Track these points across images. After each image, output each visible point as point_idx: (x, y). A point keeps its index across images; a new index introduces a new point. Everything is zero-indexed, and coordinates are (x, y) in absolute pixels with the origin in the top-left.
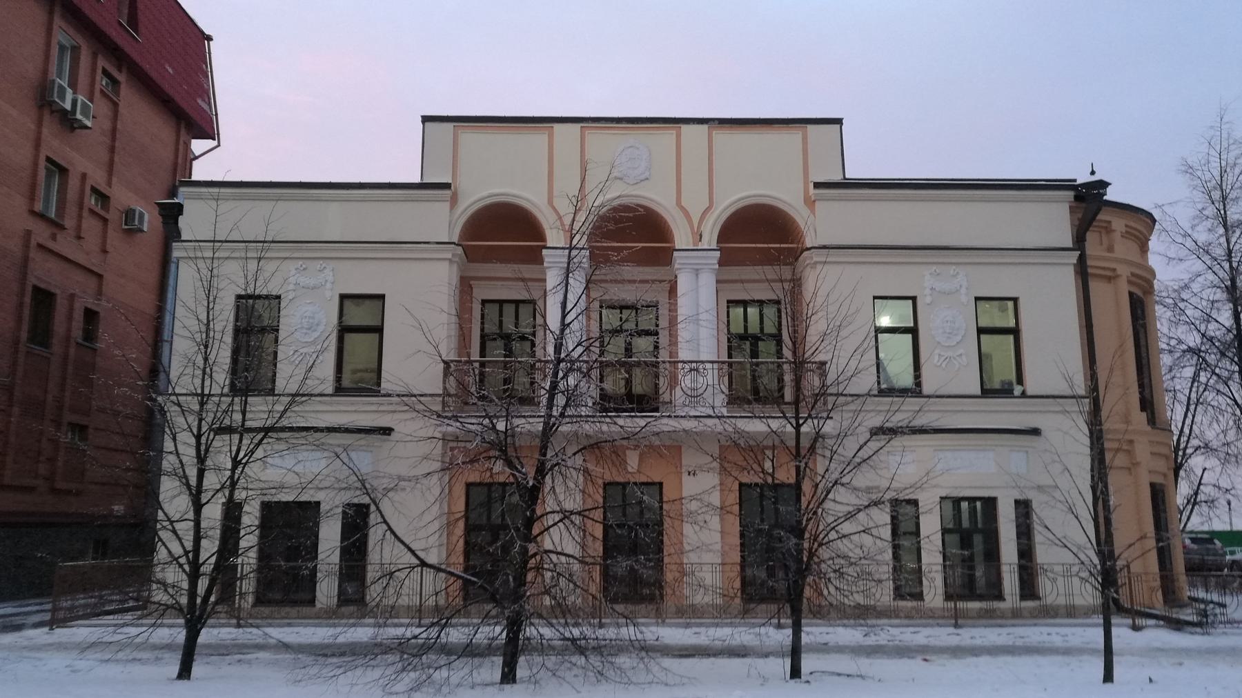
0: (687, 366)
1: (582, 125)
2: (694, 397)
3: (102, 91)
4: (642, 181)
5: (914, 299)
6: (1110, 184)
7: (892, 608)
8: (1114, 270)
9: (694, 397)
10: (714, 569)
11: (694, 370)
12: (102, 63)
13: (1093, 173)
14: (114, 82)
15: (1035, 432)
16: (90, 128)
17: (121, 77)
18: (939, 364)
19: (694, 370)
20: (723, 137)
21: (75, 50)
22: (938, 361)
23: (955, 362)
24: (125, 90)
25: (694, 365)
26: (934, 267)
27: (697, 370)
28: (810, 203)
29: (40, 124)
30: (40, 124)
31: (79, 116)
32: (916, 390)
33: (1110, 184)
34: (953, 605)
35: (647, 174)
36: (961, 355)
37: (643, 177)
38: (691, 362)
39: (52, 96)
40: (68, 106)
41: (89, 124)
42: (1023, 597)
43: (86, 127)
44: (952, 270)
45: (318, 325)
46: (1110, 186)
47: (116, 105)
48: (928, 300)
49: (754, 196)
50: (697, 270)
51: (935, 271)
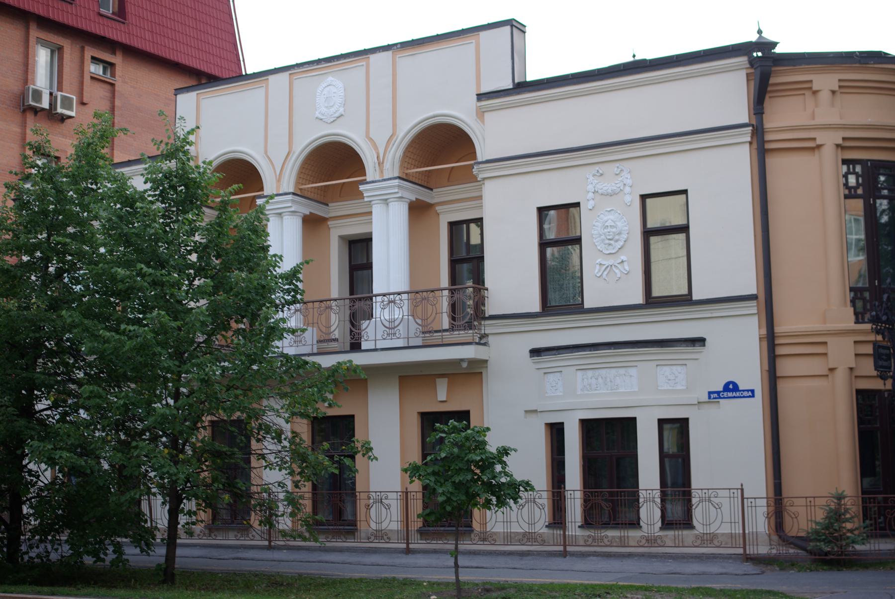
0: (386, 299)
1: (290, 72)
2: (392, 329)
3: (92, 78)
4: (338, 118)
5: (644, 197)
6: (778, 43)
7: (653, 538)
8: (814, 139)
9: (392, 329)
10: (809, 504)
11: (392, 302)
12: (90, 52)
13: (634, 56)
14: (109, 66)
15: (700, 341)
16: (73, 117)
17: (117, 59)
18: (600, 274)
19: (392, 302)
20: (408, 62)
21: (60, 49)
22: (599, 271)
23: (617, 271)
24: (119, 71)
25: (392, 297)
26: (597, 168)
27: (394, 302)
28: (480, 114)
29: (24, 125)
30: (24, 125)
31: (60, 110)
32: (685, 300)
33: (778, 43)
34: (562, 533)
35: (341, 110)
36: (623, 262)
37: (337, 115)
38: (390, 294)
39: (28, 102)
40: (45, 104)
41: (73, 114)
42: (667, 524)
43: (70, 117)
44: (614, 168)
45: (620, 234)
46: (778, 45)
47: (112, 85)
48: (591, 204)
49: (419, 123)
50: (386, 200)
51: (598, 171)
